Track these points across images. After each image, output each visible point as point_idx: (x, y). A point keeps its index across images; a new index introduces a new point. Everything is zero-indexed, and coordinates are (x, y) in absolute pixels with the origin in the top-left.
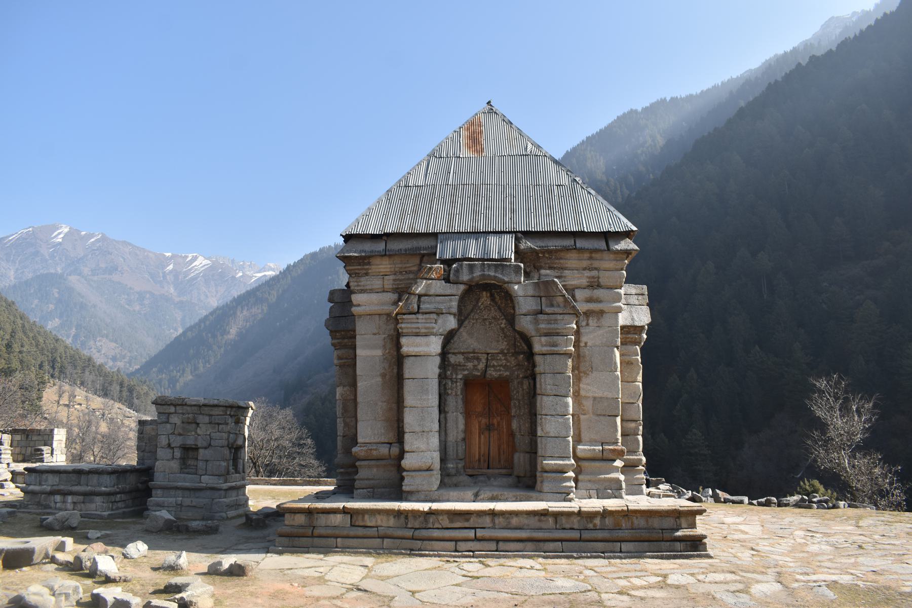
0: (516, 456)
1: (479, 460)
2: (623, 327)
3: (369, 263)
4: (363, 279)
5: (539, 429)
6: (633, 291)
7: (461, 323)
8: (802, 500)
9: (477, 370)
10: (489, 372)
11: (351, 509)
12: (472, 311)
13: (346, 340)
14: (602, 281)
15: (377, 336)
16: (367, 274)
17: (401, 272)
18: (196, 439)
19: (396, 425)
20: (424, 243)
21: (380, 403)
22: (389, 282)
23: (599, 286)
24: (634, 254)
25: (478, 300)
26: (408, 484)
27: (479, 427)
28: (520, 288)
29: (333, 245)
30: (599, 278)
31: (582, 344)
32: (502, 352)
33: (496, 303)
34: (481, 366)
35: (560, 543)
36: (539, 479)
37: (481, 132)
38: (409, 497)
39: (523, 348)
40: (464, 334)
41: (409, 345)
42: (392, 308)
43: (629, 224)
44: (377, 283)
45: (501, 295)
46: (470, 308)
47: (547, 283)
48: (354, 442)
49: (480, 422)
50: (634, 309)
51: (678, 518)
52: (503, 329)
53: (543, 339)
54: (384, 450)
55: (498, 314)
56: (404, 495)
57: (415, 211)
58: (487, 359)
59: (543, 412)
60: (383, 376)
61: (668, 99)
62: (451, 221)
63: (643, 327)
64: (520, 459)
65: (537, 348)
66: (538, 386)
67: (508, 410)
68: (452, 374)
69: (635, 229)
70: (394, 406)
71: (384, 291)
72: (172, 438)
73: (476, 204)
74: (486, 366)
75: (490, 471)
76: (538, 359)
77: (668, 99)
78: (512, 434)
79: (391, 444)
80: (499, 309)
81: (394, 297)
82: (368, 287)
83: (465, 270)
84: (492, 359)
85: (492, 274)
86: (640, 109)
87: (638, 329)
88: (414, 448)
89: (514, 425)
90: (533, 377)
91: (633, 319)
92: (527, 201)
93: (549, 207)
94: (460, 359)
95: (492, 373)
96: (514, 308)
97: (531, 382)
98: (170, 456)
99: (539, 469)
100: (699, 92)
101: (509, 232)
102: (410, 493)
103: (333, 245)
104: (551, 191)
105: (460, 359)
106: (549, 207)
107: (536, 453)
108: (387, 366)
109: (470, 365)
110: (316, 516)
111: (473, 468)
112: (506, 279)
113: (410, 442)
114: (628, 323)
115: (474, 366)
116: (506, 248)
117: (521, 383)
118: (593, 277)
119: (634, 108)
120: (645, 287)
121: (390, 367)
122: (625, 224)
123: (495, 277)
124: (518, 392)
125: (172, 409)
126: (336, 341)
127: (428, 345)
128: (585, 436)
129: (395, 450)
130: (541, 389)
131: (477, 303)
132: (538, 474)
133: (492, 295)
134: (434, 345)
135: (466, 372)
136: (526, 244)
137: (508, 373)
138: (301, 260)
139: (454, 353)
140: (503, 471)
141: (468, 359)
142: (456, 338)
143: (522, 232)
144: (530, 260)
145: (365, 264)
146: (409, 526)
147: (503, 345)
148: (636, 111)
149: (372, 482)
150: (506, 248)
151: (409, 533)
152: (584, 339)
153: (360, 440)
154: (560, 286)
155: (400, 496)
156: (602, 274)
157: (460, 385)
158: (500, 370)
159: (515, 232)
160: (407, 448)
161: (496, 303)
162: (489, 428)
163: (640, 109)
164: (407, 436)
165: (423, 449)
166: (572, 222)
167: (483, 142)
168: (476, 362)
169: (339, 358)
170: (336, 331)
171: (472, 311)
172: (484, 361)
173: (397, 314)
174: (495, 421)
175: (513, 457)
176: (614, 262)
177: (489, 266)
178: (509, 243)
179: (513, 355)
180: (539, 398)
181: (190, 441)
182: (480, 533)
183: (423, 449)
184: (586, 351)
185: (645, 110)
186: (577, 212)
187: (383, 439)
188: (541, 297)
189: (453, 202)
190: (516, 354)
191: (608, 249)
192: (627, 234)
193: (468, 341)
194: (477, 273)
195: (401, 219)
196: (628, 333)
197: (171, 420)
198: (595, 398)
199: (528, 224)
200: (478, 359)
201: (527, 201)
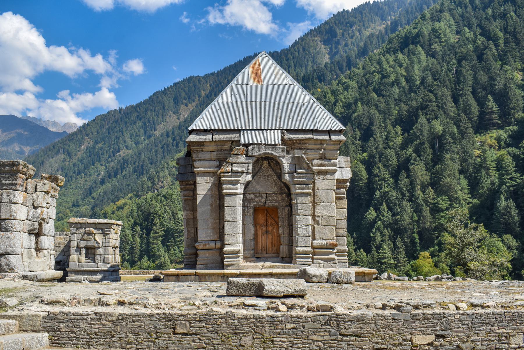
0: (281, 247)
1: (262, 250)
2: (337, 180)
3: (203, 145)
4: (200, 154)
5: (294, 232)
6: (343, 160)
7: (253, 178)
8: (438, 277)
9: (261, 202)
10: (267, 203)
11: (199, 273)
12: (259, 171)
13: (188, 186)
16: (202, 151)
17: (221, 150)
19: (218, 231)
21: (210, 220)
22: (214, 155)
24: (343, 142)
25: (262, 165)
26: (227, 261)
27: (262, 232)
28: (286, 162)
29: (118, 109)
30: (325, 154)
31: (316, 189)
32: (274, 193)
33: (271, 167)
34: (263, 200)
36: (294, 258)
37: (260, 69)
39: (287, 192)
40: (254, 183)
42: (216, 169)
43: (342, 126)
44: (207, 156)
45: (274, 163)
46: (257, 169)
47: (298, 157)
48: (196, 241)
49: (262, 230)
50: (343, 170)
51: (364, 276)
52: (275, 181)
54: (212, 245)
55: (272, 173)
57: (227, 117)
60: (211, 205)
61: (371, 2)
62: (247, 123)
63: (348, 180)
64: (284, 249)
65: (293, 191)
66: (293, 210)
67: (277, 223)
68: (248, 204)
69: (344, 128)
70: (218, 221)
71: (211, 160)
73: (260, 113)
74: (266, 200)
75: (267, 255)
76: (293, 196)
77: (371, 2)
78: (279, 236)
79: (216, 241)
80: (273, 170)
81: (217, 163)
82: (203, 158)
83: (256, 150)
85: (270, 152)
86: (350, 10)
87: (344, 181)
88: (230, 242)
89: (281, 231)
90: (290, 205)
91: (342, 175)
92: (287, 112)
93: (299, 116)
94: (252, 196)
95: (269, 204)
96: (281, 170)
97: (290, 208)
99: (294, 252)
101: (279, 130)
103: (118, 109)
105: (252, 196)
106: (299, 116)
108: (213, 200)
109: (257, 199)
110: (180, 277)
112: (277, 155)
113: (228, 239)
114: (340, 177)
115: (260, 200)
116: (275, 137)
117: (284, 209)
119: (346, 9)
120: (349, 158)
121: (215, 200)
122: (339, 126)
124: (282, 214)
126: (183, 187)
127: (236, 189)
128: (317, 236)
129: (218, 245)
130: (295, 212)
131: (261, 167)
132: (293, 255)
133: (269, 163)
134: (240, 189)
135: (255, 203)
136: (288, 136)
139: (249, 193)
140: (274, 255)
141: (256, 197)
142: (250, 186)
143: (285, 130)
144: (289, 145)
145: (201, 146)
147: (275, 189)
148: (347, 11)
150: (275, 137)
152: (317, 186)
153: (199, 239)
154: (306, 159)
155: (222, 268)
156: (327, 152)
157: (252, 210)
158: (273, 202)
159: (282, 130)
161: (271, 167)
162: (267, 232)
164: (226, 237)
165: (236, 241)
166: (312, 124)
167: (262, 76)
168: (260, 198)
169: (185, 196)
170: (182, 181)
171: (259, 171)
172: (265, 197)
173: (220, 173)
174: (270, 229)
175: (279, 248)
178: (278, 134)
179: (280, 194)
180: (294, 216)
183: (236, 241)
184: (317, 192)
185: (354, 10)
186: (314, 119)
187: (212, 239)
189: (248, 112)
190: (281, 194)
191: (330, 139)
192: (340, 132)
194: (262, 152)
195: (220, 121)
196: (340, 183)
199: (288, 125)
200: (262, 196)
201: (287, 112)
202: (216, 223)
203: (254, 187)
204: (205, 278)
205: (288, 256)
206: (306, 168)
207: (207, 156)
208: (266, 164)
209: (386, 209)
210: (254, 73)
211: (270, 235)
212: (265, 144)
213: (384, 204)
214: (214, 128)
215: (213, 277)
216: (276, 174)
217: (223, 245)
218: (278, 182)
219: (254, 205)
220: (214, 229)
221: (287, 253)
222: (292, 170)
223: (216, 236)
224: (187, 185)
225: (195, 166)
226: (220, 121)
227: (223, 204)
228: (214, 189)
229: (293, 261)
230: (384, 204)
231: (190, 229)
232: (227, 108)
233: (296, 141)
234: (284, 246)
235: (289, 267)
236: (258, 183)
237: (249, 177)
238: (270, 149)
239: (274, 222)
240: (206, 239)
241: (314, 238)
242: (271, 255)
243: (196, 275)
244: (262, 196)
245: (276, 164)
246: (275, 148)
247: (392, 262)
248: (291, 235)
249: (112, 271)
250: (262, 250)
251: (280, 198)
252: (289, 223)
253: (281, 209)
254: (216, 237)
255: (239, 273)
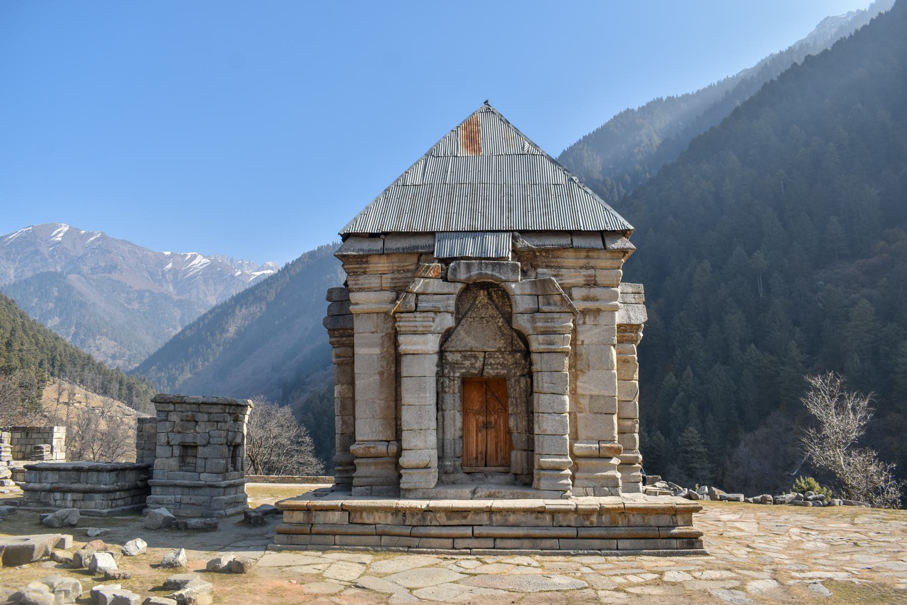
0: (513, 453)
1: (477, 458)
2: (619, 326)
3: (367, 262)
4: (361, 278)
5: (536, 427)
6: (630, 290)
8: (798, 498)
10: (486, 370)
12: (469, 309)
13: (344, 339)
14: (599, 280)
15: (375, 335)
16: (365, 273)
18: (195, 437)
20: (421, 242)
21: (378, 401)
22: (387, 281)
23: (596, 284)
25: (475, 299)
27: (477, 424)
29: (331, 244)
30: (595, 276)
31: (579, 343)
32: (499, 351)
33: (493, 302)
34: (479, 364)
35: (557, 540)
36: (536, 477)
37: (479, 131)
38: (407, 495)
39: (521, 347)
40: (462, 332)
41: (407, 344)
42: (389, 306)
43: (626, 223)
44: (375, 282)
45: (495, 291)
47: (544, 282)
49: (477, 420)
50: (630, 308)
51: (675, 515)
52: (500, 328)
53: (540, 337)
54: (382, 448)
55: (495, 313)
56: (402, 493)
57: (412, 210)
58: (485, 357)
59: (541, 410)
60: (381, 374)
61: (664, 98)
62: (448, 220)
63: (639, 325)
64: (517, 457)
65: (534, 346)
66: (535, 384)
67: (505, 408)
68: (449, 372)
69: (631, 227)
70: (392, 404)
71: (382, 290)
72: (171, 436)
74: (484, 364)
75: (488, 468)
76: (535, 357)
77: (664, 98)
78: (509, 432)
79: (389, 441)
80: (497, 307)
82: (366, 286)
83: (463, 269)
84: (490, 358)
85: (489, 272)
86: (636, 109)
87: (634, 328)
89: (512, 423)
91: (629, 318)
93: (546, 206)
94: (457, 357)
95: (490, 372)
96: (511, 306)
97: (529, 380)
98: (169, 454)
99: (536, 466)
100: (695, 91)
101: (506, 231)
102: (408, 490)
103: (331, 244)
104: (548, 191)
107: (533, 451)
108: (385, 364)
109: (467, 363)
111: (471, 466)
112: (503, 278)
113: (408, 439)
115: (472, 364)
116: (503, 246)
117: (519, 381)
118: (590, 276)
119: (631, 108)
120: (641, 285)
121: (388, 364)
122: (621, 222)
123: (493, 275)
124: (515, 390)
125: (171, 407)
126: (334, 339)
127: (425, 343)
128: (582, 433)
132: (535, 472)
133: (489, 294)
134: (432, 343)
135: (464, 371)
136: (524, 243)
137: (505, 371)
138: (300, 259)
139: (451, 352)
140: (501, 469)
142: (453, 337)
144: (527, 260)
145: (363, 263)
146: (407, 523)
147: (501, 344)
148: (633, 110)
149: (370, 479)
150: (503, 246)
151: (407, 531)
152: (581, 337)
153: (358, 438)
156: (598, 272)
157: (457, 383)
158: (497, 368)
159: (513, 231)
160: (404, 446)
161: (493, 302)
162: (487, 426)
163: (636, 109)
168: (473, 361)
170: (334, 330)
171: (469, 309)
172: (482, 359)
173: (395, 313)
174: (492, 419)
175: (510, 455)
176: (611, 261)
177: (487, 264)
178: (506, 241)
179: (510, 353)
180: (536, 396)
181: (189, 440)
182: (477, 531)
184: (582, 350)
185: (642, 109)
186: (574, 211)
187: (381, 437)
188: (538, 296)
189: (450, 202)
190: (513, 352)
192: (624, 233)
193: (465, 339)
194: (475, 272)
196: (625, 331)
197: (170, 418)
198: (591, 396)
200: (476, 357)
202: (388, 407)
203: (462, 340)
204: (361, 514)
205: (526, 472)
206: (559, 303)
207: (375, 282)
208: (482, 292)
209: (691, 375)
210: (467, 137)
211: (493, 430)
212: (480, 258)
213: (689, 367)
214: (387, 229)
215: (376, 514)
216: (503, 315)
217: (400, 451)
218: (507, 331)
219: (462, 374)
220: (385, 418)
221: (525, 465)
222: (531, 306)
223: (389, 432)
224: (342, 337)
225: (353, 301)
226: (399, 217)
227: (400, 373)
228: (387, 344)
229: (535, 484)
230: (689, 367)
231: (346, 418)
232: (414, 195)
233: (539, 249)
234: (519, 453)
235: (525, 497)
236: (468, 333)
237: (449, 321)
238: (490, 267)
239: (500, 407)
240: (370, 438)
241: (575, 438)
242: (494, 469)
243: (342, 510)
244: (476, 357)
245: (503, 296)
246: (500, 264)
247: (701, 449)
248: (530, 430)
249: (225, 487)
250: (477, 458)
251: (510, 360)
252: (527, 409)
253: (513, 381)
254: (389, 434)
255: (424, 507)
